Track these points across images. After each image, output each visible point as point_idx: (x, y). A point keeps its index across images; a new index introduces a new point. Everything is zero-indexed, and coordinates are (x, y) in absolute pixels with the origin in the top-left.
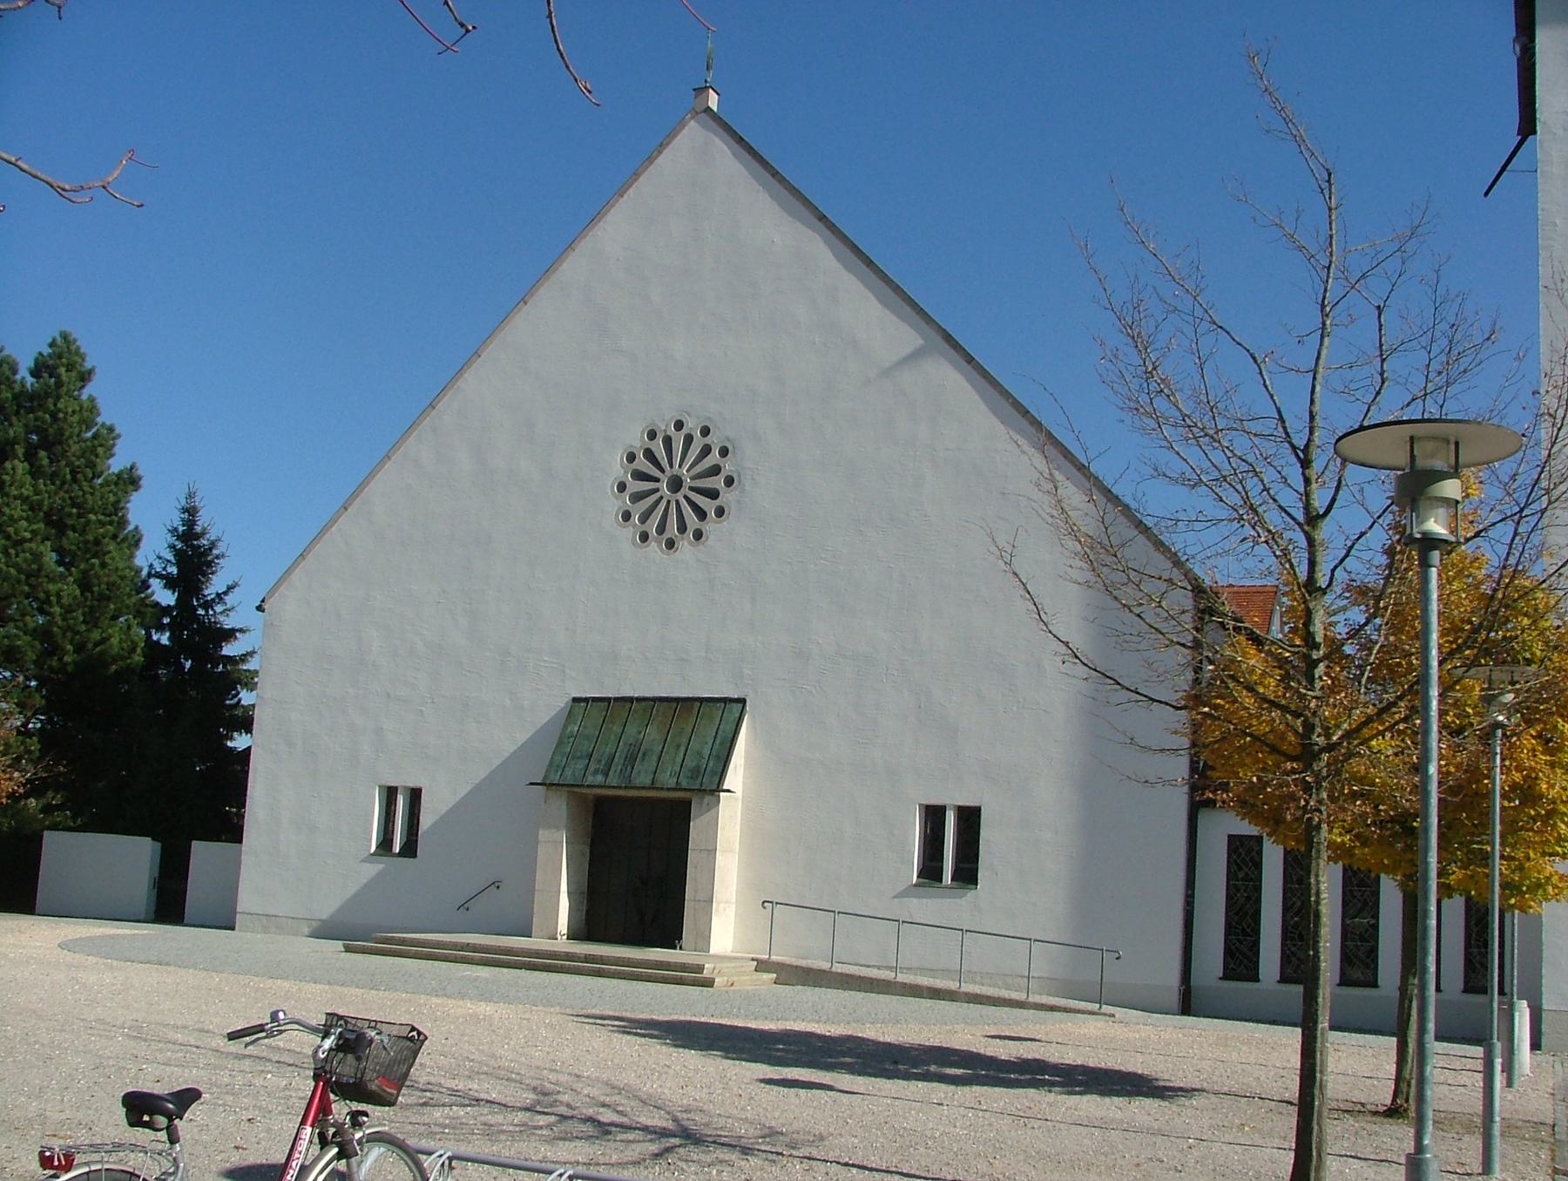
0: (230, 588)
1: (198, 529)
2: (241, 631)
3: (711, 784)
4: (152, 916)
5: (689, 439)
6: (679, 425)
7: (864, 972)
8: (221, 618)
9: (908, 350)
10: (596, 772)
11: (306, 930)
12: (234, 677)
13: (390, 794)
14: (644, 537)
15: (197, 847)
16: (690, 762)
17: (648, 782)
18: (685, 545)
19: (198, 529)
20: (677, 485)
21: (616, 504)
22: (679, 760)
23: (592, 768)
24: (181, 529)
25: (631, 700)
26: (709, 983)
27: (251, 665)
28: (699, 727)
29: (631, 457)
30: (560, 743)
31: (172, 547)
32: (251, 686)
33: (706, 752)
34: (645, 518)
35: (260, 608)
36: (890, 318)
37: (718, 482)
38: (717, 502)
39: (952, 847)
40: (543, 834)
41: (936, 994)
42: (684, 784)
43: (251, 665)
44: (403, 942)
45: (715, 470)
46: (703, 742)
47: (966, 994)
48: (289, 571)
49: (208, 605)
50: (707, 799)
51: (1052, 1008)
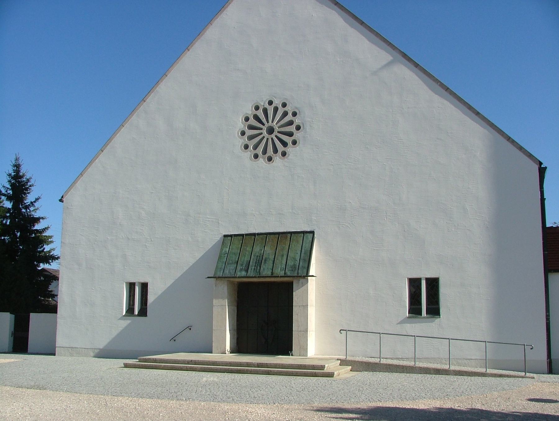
0: (37, 200)
1: (21, 174)
2: (43, 218)
3: (304, 275)
4: (12, 350)
5: (276, 109)
6: (270, 103)
7: (401, 363)
8: (33, 213)
9: (385, 63)
10: (241, 270)
11: (92, 354)
12: (40, 239)
13: (131, 286)
14: (256, 156)
15: (33, 316)
16: (290, 263)
17: (269, 273)
18: (277, 159)
19: (21, 174)
20: (272, 131)
21: (240, 141)
22: (284, 262)
23: (239, 267)
24: (13, 174)
25: (254, 235)
26: (331, 375)
27: (46, 234)
28: (296, 245)
29: (247, 119)
30: (220, 257)
31: (10, 181)
32: (49, 243)
33: (298, 258)
34: (255, 147)
35: (61, 200)
36: (374, 47)
37: (292, 128)
38: (293, 138)
39: (425, 298)
40: (215, 302)
41: (438, 372)
42: (289, 273)
43: (46, 234)
44: (155, 361)
45: (291, 123)
46: (295, 253)
47: (454, 371)
48: (75, 182)
49: (27, 207)
50: (302, 280)
51: (501, 376)
